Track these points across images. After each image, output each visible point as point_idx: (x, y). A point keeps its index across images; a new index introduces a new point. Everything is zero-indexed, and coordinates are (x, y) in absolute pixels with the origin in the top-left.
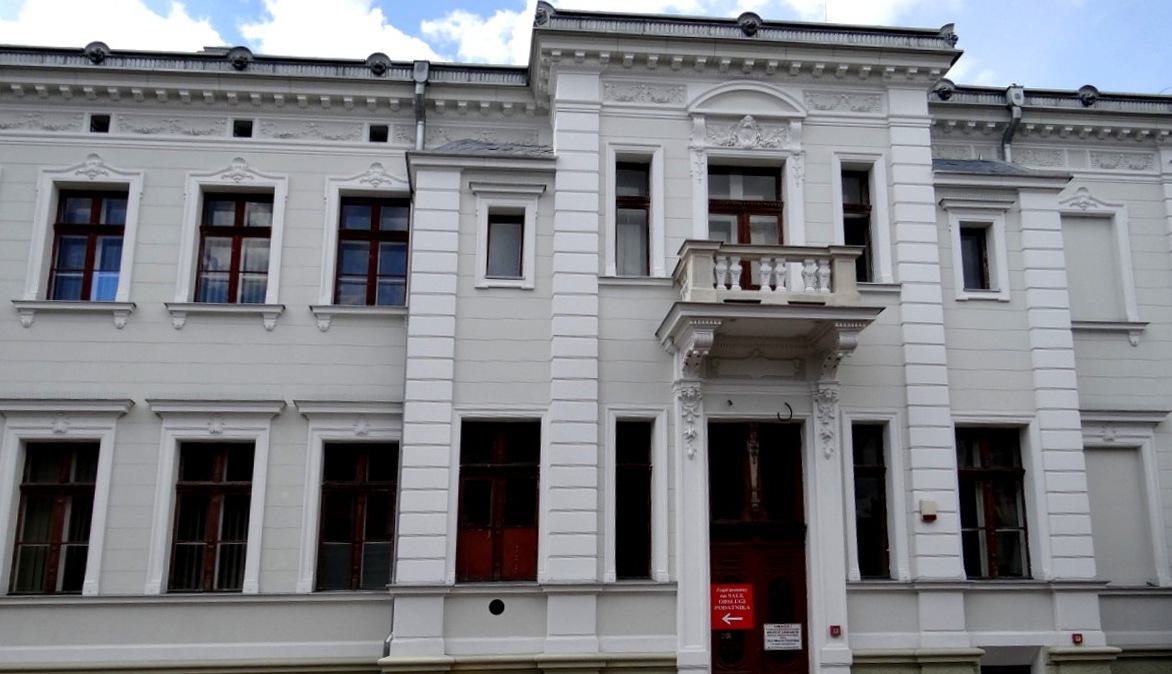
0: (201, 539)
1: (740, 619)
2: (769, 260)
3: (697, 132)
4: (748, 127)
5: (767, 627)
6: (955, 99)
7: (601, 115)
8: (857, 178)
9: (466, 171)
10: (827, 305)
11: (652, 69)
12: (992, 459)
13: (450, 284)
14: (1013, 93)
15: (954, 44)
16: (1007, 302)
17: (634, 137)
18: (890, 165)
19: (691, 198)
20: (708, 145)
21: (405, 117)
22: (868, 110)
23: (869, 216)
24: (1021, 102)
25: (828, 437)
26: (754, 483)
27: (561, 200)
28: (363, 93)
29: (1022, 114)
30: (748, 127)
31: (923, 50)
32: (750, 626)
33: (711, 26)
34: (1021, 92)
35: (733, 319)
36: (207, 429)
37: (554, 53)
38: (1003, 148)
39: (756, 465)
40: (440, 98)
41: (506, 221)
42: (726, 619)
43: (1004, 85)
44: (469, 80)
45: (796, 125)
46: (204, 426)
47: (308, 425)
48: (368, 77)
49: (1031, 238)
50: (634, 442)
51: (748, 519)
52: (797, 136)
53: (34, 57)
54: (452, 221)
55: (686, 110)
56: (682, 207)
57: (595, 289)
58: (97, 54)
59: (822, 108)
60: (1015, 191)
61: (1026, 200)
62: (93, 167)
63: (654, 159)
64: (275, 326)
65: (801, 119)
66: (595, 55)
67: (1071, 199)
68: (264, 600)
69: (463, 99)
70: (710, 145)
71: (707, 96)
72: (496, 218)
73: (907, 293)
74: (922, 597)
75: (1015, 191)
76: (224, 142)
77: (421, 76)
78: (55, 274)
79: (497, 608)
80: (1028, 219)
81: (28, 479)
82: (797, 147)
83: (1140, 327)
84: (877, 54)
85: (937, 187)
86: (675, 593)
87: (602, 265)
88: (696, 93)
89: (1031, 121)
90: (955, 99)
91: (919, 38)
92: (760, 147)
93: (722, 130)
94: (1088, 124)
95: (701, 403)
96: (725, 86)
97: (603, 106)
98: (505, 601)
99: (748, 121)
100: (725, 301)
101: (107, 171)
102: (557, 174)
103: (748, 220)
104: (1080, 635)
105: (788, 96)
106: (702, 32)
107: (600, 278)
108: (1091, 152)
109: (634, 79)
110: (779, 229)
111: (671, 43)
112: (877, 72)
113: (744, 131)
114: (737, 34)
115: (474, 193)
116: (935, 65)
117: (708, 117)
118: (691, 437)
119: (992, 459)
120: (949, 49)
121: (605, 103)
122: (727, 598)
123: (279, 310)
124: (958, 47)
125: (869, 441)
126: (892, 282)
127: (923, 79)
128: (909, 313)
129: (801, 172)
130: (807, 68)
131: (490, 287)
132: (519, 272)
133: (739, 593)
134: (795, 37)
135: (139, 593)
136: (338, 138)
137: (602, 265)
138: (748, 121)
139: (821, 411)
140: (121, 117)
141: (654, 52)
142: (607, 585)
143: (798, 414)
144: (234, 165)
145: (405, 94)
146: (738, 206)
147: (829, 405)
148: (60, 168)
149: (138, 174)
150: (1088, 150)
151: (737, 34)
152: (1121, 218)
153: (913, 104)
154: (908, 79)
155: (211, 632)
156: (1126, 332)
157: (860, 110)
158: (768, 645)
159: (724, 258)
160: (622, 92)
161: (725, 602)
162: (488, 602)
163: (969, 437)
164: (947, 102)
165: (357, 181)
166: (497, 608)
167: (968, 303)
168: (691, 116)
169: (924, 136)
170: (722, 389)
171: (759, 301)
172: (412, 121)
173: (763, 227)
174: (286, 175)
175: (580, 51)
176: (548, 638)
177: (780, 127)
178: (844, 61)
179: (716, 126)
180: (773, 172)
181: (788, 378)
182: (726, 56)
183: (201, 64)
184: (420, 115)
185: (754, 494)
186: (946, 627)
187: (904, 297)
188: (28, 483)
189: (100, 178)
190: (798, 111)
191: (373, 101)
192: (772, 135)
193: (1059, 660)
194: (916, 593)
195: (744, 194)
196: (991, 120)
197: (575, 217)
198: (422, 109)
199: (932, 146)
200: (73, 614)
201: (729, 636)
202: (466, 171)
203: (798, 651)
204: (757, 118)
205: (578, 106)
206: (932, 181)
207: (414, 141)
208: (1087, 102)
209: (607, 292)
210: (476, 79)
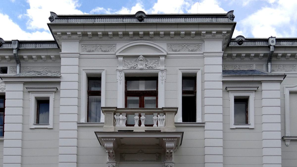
2: (138, 114)
3: (120, 63)
4: (141, 60)
6: (245, 44)
7: (79, 58)
8: (189, 80)
11: (100, 38)
13: (220, 126)
14: (270, 40)
15: (233, 19)
16: (52, 129)
17: (94, 66)
18: (203, 74)
21: (12, 63)
22: (196, 51)
23: (196, 95)
24: (274, 44)
27: (62, 93)
29: (274, 49)
30: (141, 60)
31: (222, 24)
33: (123, 18)
35: (122, 138)
37: (58, 34)
38: (268, 64)
40: (25, 55)
43: (266, 37)
45: (162, 59)
49: (268, 101)
52: (164, 63)
54: (20, 103)
55: (115, 54)
56: (114, 94)
57: (76, 128)
59: (176, 51)
61: (265, 86)
63: (102, 74)
65: (165, 56)
66: (75, 33)
69: (34, 55)
70: (126, 69)
72: (238, 100)
73: (207, 126)
75: (260, 82)
77: (16, 46)
80: (265, 94)
82: (163, 68)
85: (223, 82)
87: (79, 118)
88: (120, 47)
89: (280, 52)
90: (245, 44)
91: (217, 18)
92: (147, 69)
93: (131, 62)
96: (131, 44)
97: (80, 54)
99: (141, 58)
100: (118, 131)
102: (61, 83)
103: (144, 99)
105: (160, 47)
106: (120, 21)
107: (78, 123)
112: (198, 34)
113: (140, 62)
114: (135, 21)
115: (29, 92)
116: (225, 30)
117: (124, 57)
120: (230, 21)
121: (81, 53)
124: (235, 21)
126: (201, 122)
127: (219, 36)
128: (207, 134)
129: (164, 78)
130: (167, 34)
131: (35, 128)
132: (247, 122)
134: (167, 20)
137: (79, 118)
138: (141, 58)
141: (100, 31)
146: (133, 93)
148: (291, 86)
150: (254, 64)
151: (135, 21)
153: (216, 47)
154: (213, 36)
157: (192, 51)
160: (89, 48)
167: (35, 129)
168: (118, 57)
169: (220, 60)
171: (133, 131)
172: (15, 65)
173: (149, 102)
177: (156, 60)
178: (183, 30)
179: (128, 61)
180: (154, 78)
182: (131, 30)
184: (18, 62)
187: (206, 128)
195: (145, 88)
196: (262, 52)
197: (69, 100)
198: (18, 60)
199: (222, 65)
202: (25, 83)
204: (145, 56)
205: (70, 55)
206: (222, 79)
207: (16, 72)
209: (81, 129)
210: (38, 46)
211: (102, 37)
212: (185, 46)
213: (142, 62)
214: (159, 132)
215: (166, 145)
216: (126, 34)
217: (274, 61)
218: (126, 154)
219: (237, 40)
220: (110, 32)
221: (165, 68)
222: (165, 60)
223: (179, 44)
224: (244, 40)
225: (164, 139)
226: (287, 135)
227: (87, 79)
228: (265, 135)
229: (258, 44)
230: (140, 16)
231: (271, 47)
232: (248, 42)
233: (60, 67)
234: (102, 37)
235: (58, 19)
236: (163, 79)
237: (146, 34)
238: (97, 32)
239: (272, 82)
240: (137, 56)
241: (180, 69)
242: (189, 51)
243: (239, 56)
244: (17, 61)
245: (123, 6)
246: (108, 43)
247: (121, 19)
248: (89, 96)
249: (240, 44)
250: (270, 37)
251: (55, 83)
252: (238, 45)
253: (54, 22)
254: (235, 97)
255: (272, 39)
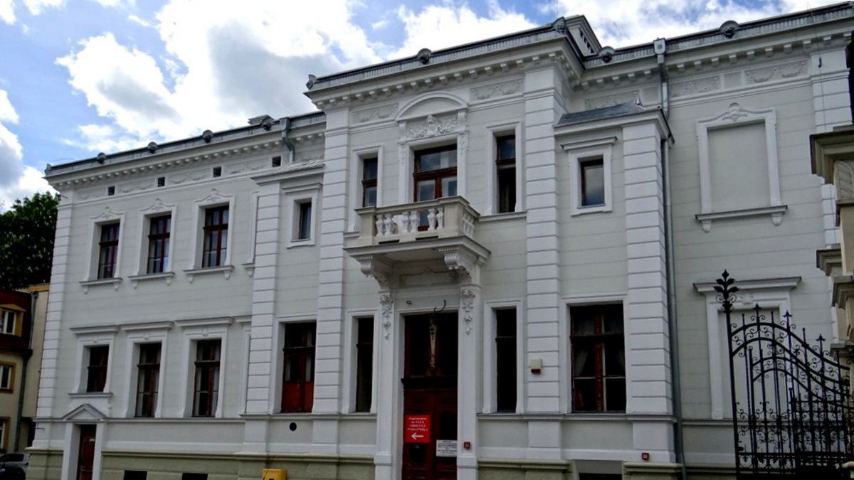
0: (207, 390)
1: (422, 436)
3: (402, 133)
4: (431, 123)
5: (438, 442)
6: (615, 60)
8: (505, 142)
9: (282, 182)
10: (439, 237)
12: (596, 330)
17: (366, 144)
19: (398, 176)
20: (408, 139)
25: (468, 320)
26: (433, 351)
27: (327, 190)
28: (690, 59)
29: (665, 59)
30: (431, 123)
32: (427, 441)
34: (663, 43)
36: (201, 334)
39: (434, 340)
40: (298, 136)
41: (305, 207)
42: (414, 436)
44: (760, 32)
45: (461, 115)
46: (201, 332)
47: (706, 299)
48: (263, 133)
49: (633, 158)
50: (365, 327)
51: (429, 374)
53: (305, 120)
56: (396, 183)
58: (208, 137)
60: (620, 128)
61: (627, 133)
62: (735, 112)
64: (782, 221)
65: (466, 110)
67: (723, 115)
68: (226, 422)
70: (410, 139)
71: (404, 110)
72: (585, 164)
74: (315, 423)
75: (620, 128)
76: (722, 93)
77: (660, 51)
78: (152, 260)
79: (293, 427)
80: (628, 147)
81: (201, 357)
82: (462, 129)
83: (783, 210)
84: (445, 67)
85: (557, 137)
86: (375, 420)
87: (347, 226)
88: (404, 104)
89: (680, 62)
90: (615, 60)
93: (418, 127)
94: (732, 52)
95: (393, 305)
97: (350, 128)
98: (297, 424)
101: (746, 113)
104: (648, 454)
105: (457, 97)
106: (396, 70)
108: (746, 72)
109: (369, 107)
110: (453, 186)
111: (512, 52)
114: (417, 65)
117: (408, 121)
118: (387, 326)
119: (596, 330)
121: (351, 126)
122: (415, 424)
123: (784, 210)
125: (506, 320)
128: (531, 230)
131: (581, 214)
133: (422, 421)
135: (174, 417)
136: (258, 168)
139: (464, 304)
140: (749, 73)
141: (371, 89)
142: (345, 415)
143: (451, 307)
144: (212, 193)
145: (654, 66)
147: (467, 301)
149: (770, 111)
150: (743, 71)
151: (417, 65)
152: (770, 125)
155: (599, 443)
156: (769, 215)
158: (438, 454)
159: (433, 210)
160: (362, 116)
161: (413, 426)
162: (288, 424)
163: (580, 314)
164: (271, 131)
165: (720, 119)
166: (293, 427)
168: (399, 122)
170: (405, 295)
171: (398, 241)
174: (175, 204)
175: (535, 56)
176: (245, 444)
178: (487, 65)
181: (445, 284)
183: (192, 143)
184: (664, 78)
185: (433, 359)
186: (542, 445)
188: (144, 363)
189: (110, 218)
190: (461, 105)
191: (633, 75)
192: (448, 124)
193: (634, 471)
194: (527, 421)
198: (290, 145)
200: (149, 427)
201: (417, 447)
203: (435, 453)
205: (338, 131)
206: (553, 133)
208: (268, 127)
211: (390, 94)
212: (497, 87)
213: (434, 125)
214: (435, 238)
215: (445, 259)
216: (407, 87)
217: (674, 78)
218: (408, 275)
219: (204, 136)
220: (385, 88)
221: (467, 129)
222: (466, 117)
223: (366, 110)
224: (612, 52)
225: (440, 250)
226: (703, 212)
227: (495, 139)
228: (630, 221)
229: (637, 55)
230: (424, 57)
231: (659, 56)
232: (620, 54)
233: (324, 149)
234: (476, 76)
235: (318, 83)
236: (464, 147)
237: (436, 81)
238: (468, 71)
239: (641, 124)
240: (425, 118)
241: (488, 127)
242: (504, 94)
243: (608, 80)
244: (289, 147)
245: (525, 14)
246: (487, 83)
247: (399, 66)
248: (367, 189)
249: (607, 62)
250: (656, 39)
251: (315, 176)
252: (603, 64)
253: (312, 90)
254: (579, 159)
255: (659, 43)
